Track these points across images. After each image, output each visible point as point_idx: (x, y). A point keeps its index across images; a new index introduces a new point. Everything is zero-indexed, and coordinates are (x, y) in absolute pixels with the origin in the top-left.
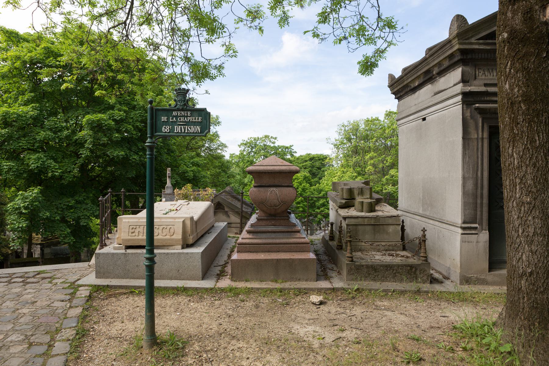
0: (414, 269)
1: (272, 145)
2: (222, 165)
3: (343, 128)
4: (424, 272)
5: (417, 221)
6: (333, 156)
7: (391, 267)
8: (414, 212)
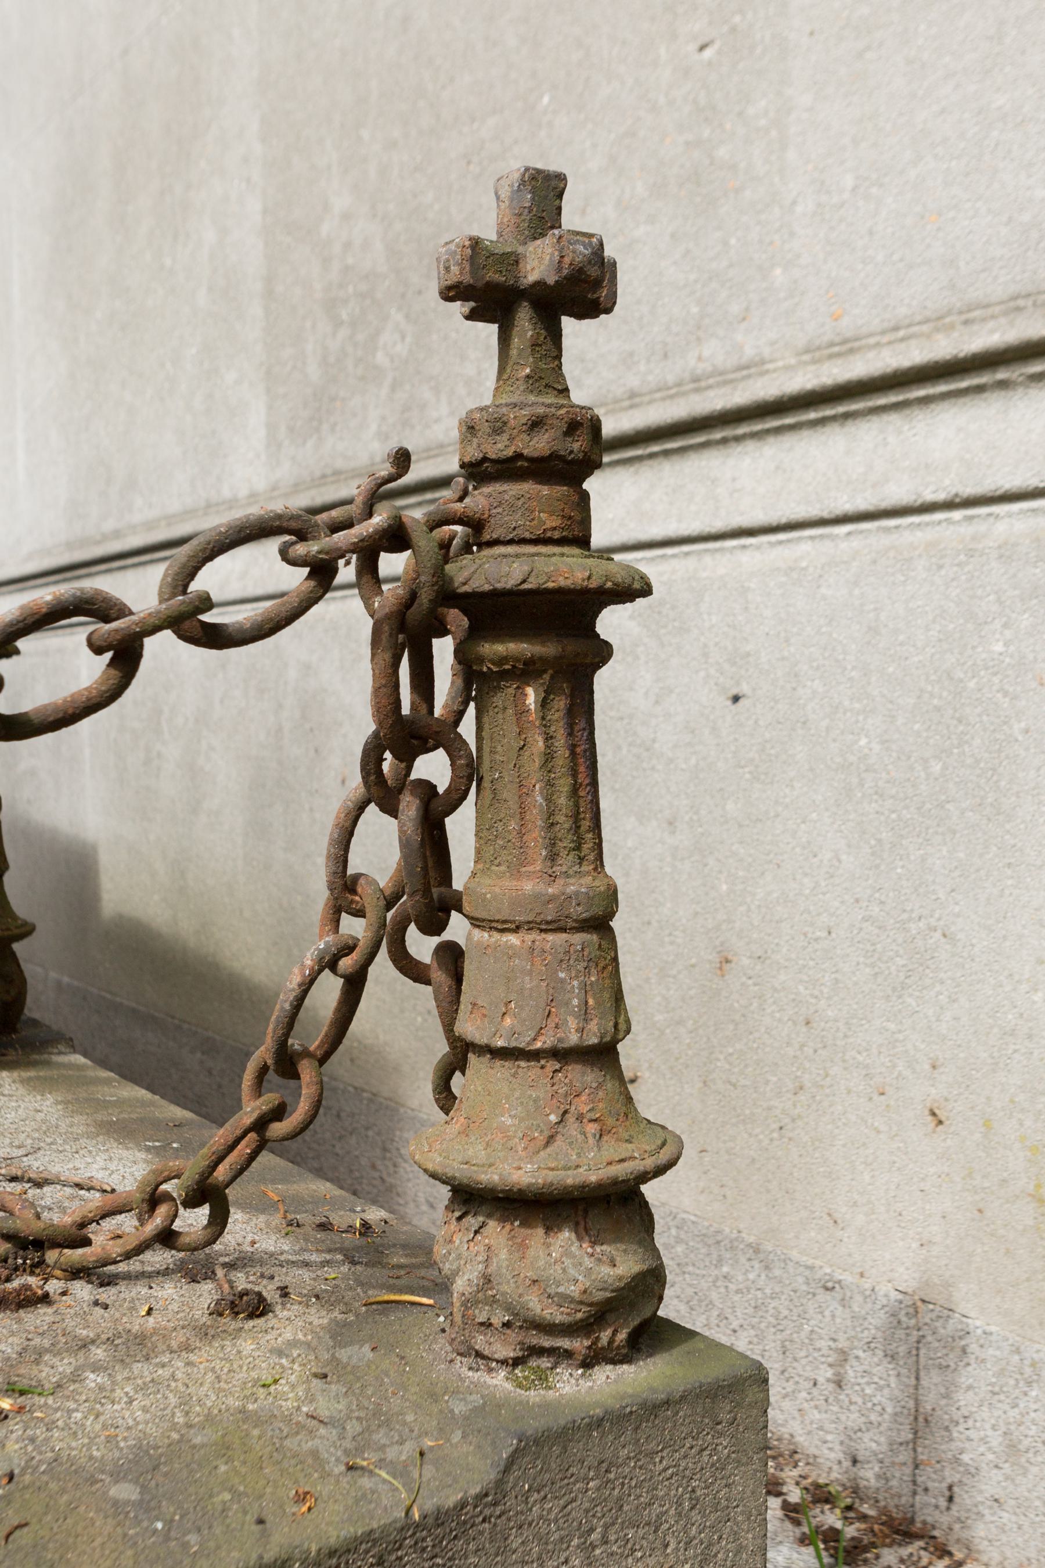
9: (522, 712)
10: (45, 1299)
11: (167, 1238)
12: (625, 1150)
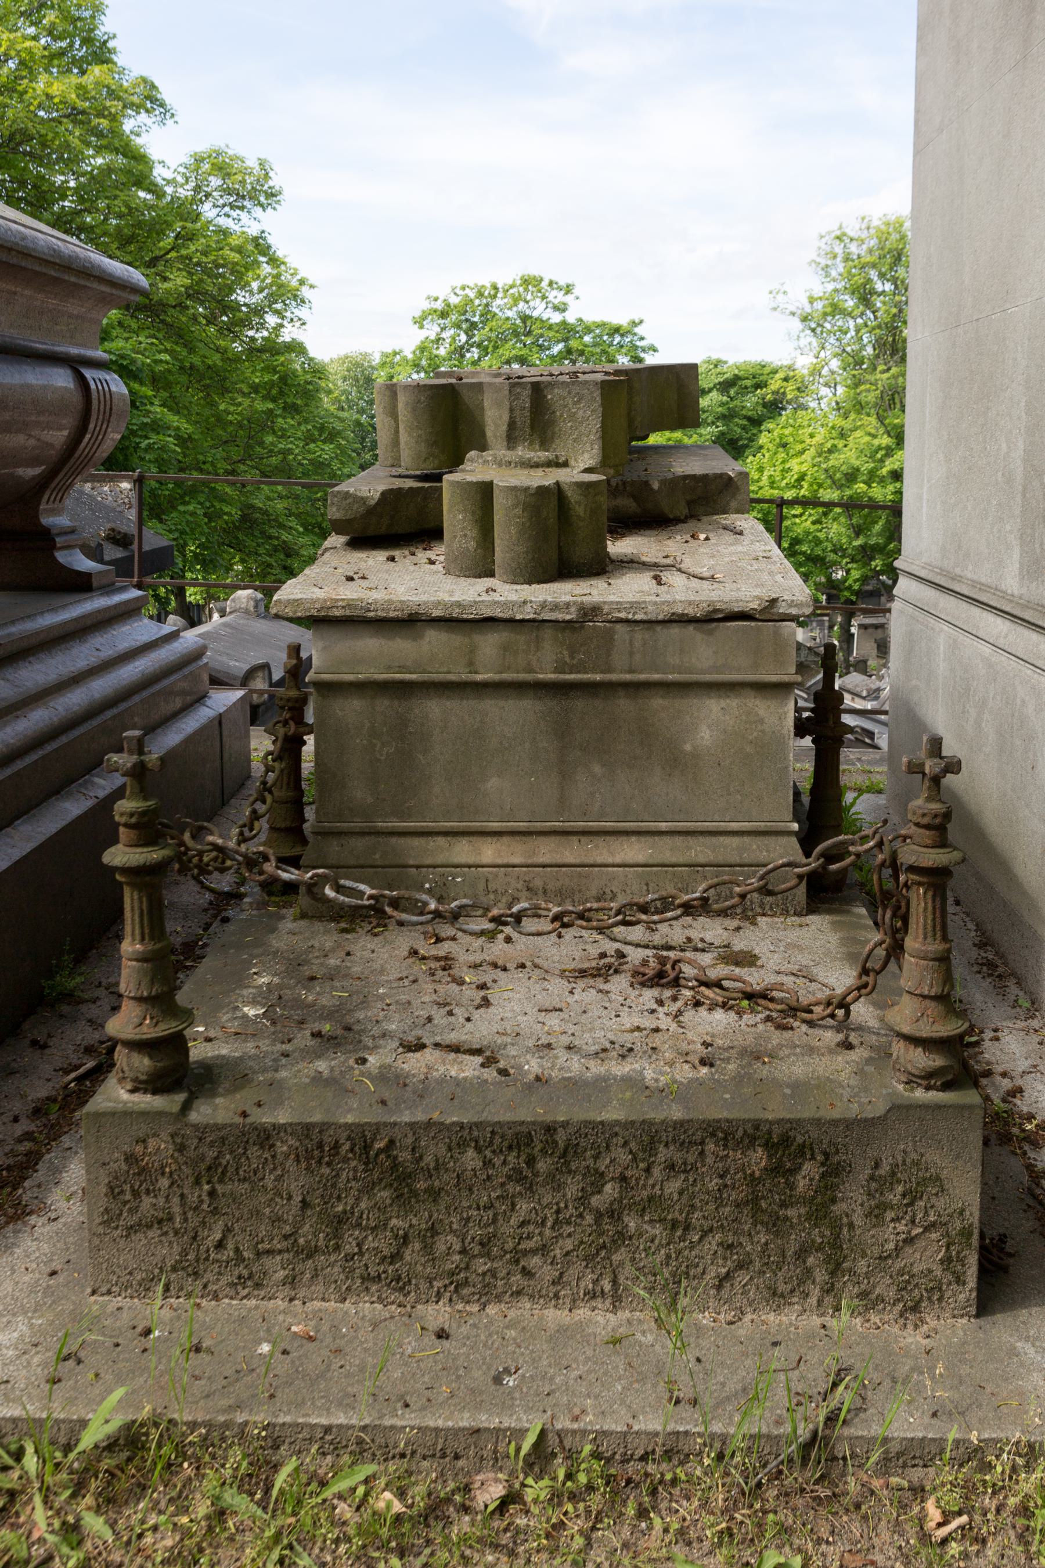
0: (809, 1171)
1: (556, 318)
2: (284, 379)
3: (839, 249)
4: (912, 1197)
5: (986, 650)
6: (804, 363)
7: (569, 1152)
8: (974, 584)
9: (918, 895)
10: (792, 1028)
11: (832, 1016)
12: (942, 1028)
